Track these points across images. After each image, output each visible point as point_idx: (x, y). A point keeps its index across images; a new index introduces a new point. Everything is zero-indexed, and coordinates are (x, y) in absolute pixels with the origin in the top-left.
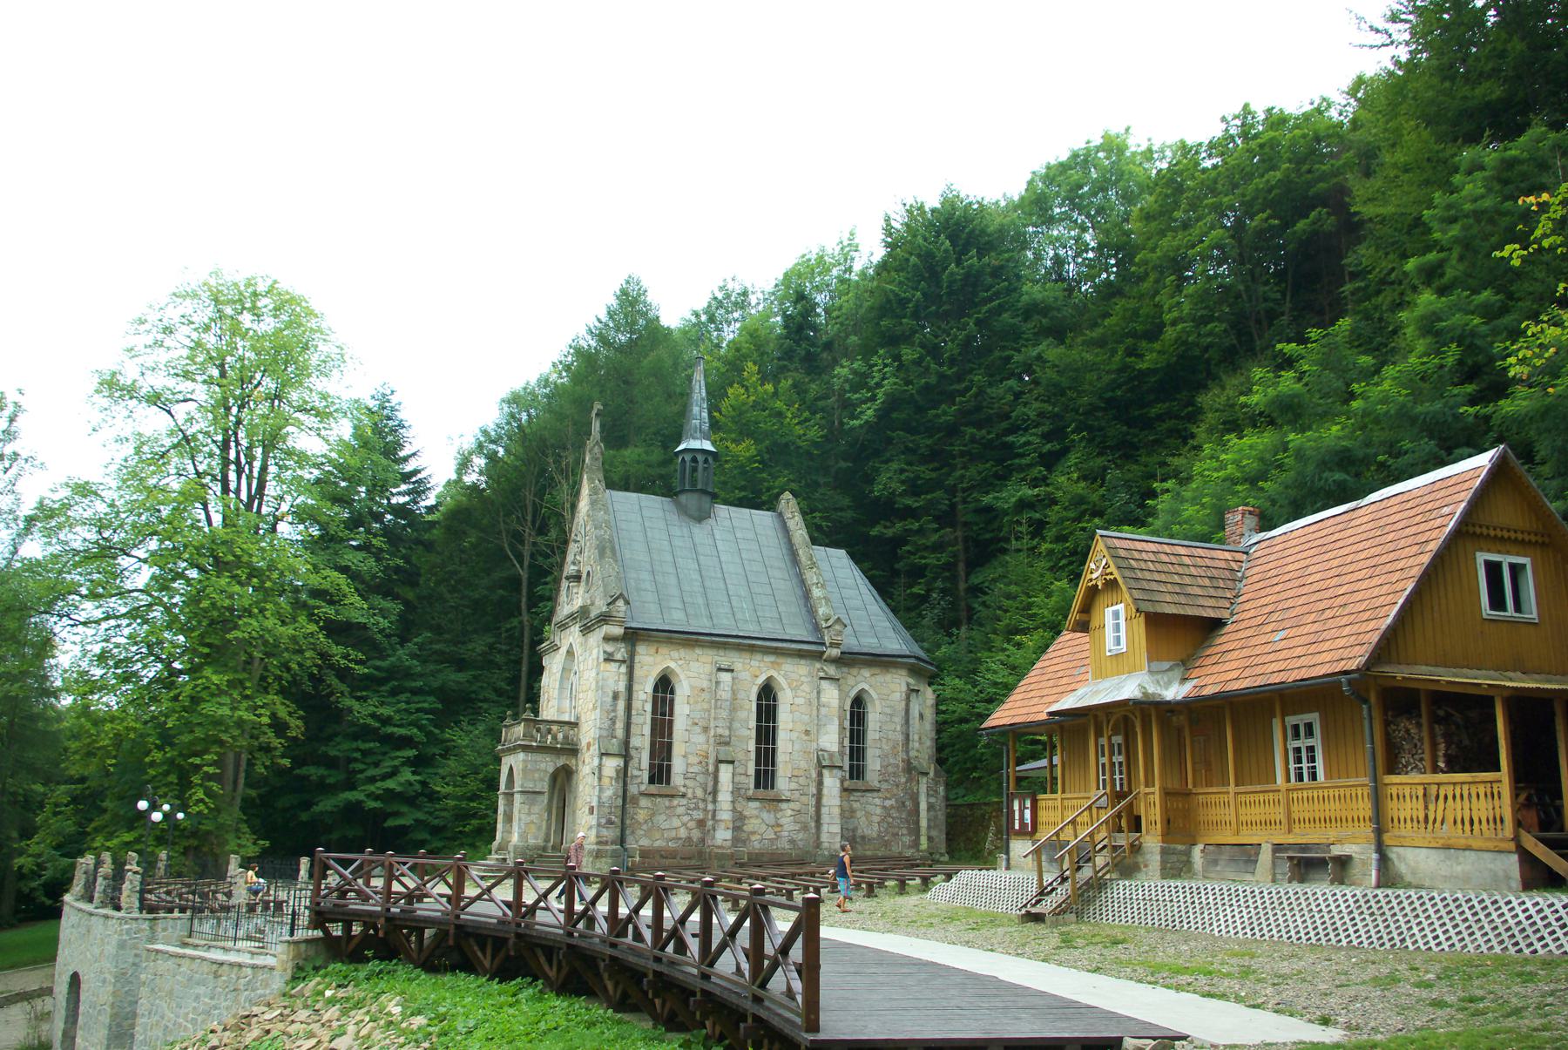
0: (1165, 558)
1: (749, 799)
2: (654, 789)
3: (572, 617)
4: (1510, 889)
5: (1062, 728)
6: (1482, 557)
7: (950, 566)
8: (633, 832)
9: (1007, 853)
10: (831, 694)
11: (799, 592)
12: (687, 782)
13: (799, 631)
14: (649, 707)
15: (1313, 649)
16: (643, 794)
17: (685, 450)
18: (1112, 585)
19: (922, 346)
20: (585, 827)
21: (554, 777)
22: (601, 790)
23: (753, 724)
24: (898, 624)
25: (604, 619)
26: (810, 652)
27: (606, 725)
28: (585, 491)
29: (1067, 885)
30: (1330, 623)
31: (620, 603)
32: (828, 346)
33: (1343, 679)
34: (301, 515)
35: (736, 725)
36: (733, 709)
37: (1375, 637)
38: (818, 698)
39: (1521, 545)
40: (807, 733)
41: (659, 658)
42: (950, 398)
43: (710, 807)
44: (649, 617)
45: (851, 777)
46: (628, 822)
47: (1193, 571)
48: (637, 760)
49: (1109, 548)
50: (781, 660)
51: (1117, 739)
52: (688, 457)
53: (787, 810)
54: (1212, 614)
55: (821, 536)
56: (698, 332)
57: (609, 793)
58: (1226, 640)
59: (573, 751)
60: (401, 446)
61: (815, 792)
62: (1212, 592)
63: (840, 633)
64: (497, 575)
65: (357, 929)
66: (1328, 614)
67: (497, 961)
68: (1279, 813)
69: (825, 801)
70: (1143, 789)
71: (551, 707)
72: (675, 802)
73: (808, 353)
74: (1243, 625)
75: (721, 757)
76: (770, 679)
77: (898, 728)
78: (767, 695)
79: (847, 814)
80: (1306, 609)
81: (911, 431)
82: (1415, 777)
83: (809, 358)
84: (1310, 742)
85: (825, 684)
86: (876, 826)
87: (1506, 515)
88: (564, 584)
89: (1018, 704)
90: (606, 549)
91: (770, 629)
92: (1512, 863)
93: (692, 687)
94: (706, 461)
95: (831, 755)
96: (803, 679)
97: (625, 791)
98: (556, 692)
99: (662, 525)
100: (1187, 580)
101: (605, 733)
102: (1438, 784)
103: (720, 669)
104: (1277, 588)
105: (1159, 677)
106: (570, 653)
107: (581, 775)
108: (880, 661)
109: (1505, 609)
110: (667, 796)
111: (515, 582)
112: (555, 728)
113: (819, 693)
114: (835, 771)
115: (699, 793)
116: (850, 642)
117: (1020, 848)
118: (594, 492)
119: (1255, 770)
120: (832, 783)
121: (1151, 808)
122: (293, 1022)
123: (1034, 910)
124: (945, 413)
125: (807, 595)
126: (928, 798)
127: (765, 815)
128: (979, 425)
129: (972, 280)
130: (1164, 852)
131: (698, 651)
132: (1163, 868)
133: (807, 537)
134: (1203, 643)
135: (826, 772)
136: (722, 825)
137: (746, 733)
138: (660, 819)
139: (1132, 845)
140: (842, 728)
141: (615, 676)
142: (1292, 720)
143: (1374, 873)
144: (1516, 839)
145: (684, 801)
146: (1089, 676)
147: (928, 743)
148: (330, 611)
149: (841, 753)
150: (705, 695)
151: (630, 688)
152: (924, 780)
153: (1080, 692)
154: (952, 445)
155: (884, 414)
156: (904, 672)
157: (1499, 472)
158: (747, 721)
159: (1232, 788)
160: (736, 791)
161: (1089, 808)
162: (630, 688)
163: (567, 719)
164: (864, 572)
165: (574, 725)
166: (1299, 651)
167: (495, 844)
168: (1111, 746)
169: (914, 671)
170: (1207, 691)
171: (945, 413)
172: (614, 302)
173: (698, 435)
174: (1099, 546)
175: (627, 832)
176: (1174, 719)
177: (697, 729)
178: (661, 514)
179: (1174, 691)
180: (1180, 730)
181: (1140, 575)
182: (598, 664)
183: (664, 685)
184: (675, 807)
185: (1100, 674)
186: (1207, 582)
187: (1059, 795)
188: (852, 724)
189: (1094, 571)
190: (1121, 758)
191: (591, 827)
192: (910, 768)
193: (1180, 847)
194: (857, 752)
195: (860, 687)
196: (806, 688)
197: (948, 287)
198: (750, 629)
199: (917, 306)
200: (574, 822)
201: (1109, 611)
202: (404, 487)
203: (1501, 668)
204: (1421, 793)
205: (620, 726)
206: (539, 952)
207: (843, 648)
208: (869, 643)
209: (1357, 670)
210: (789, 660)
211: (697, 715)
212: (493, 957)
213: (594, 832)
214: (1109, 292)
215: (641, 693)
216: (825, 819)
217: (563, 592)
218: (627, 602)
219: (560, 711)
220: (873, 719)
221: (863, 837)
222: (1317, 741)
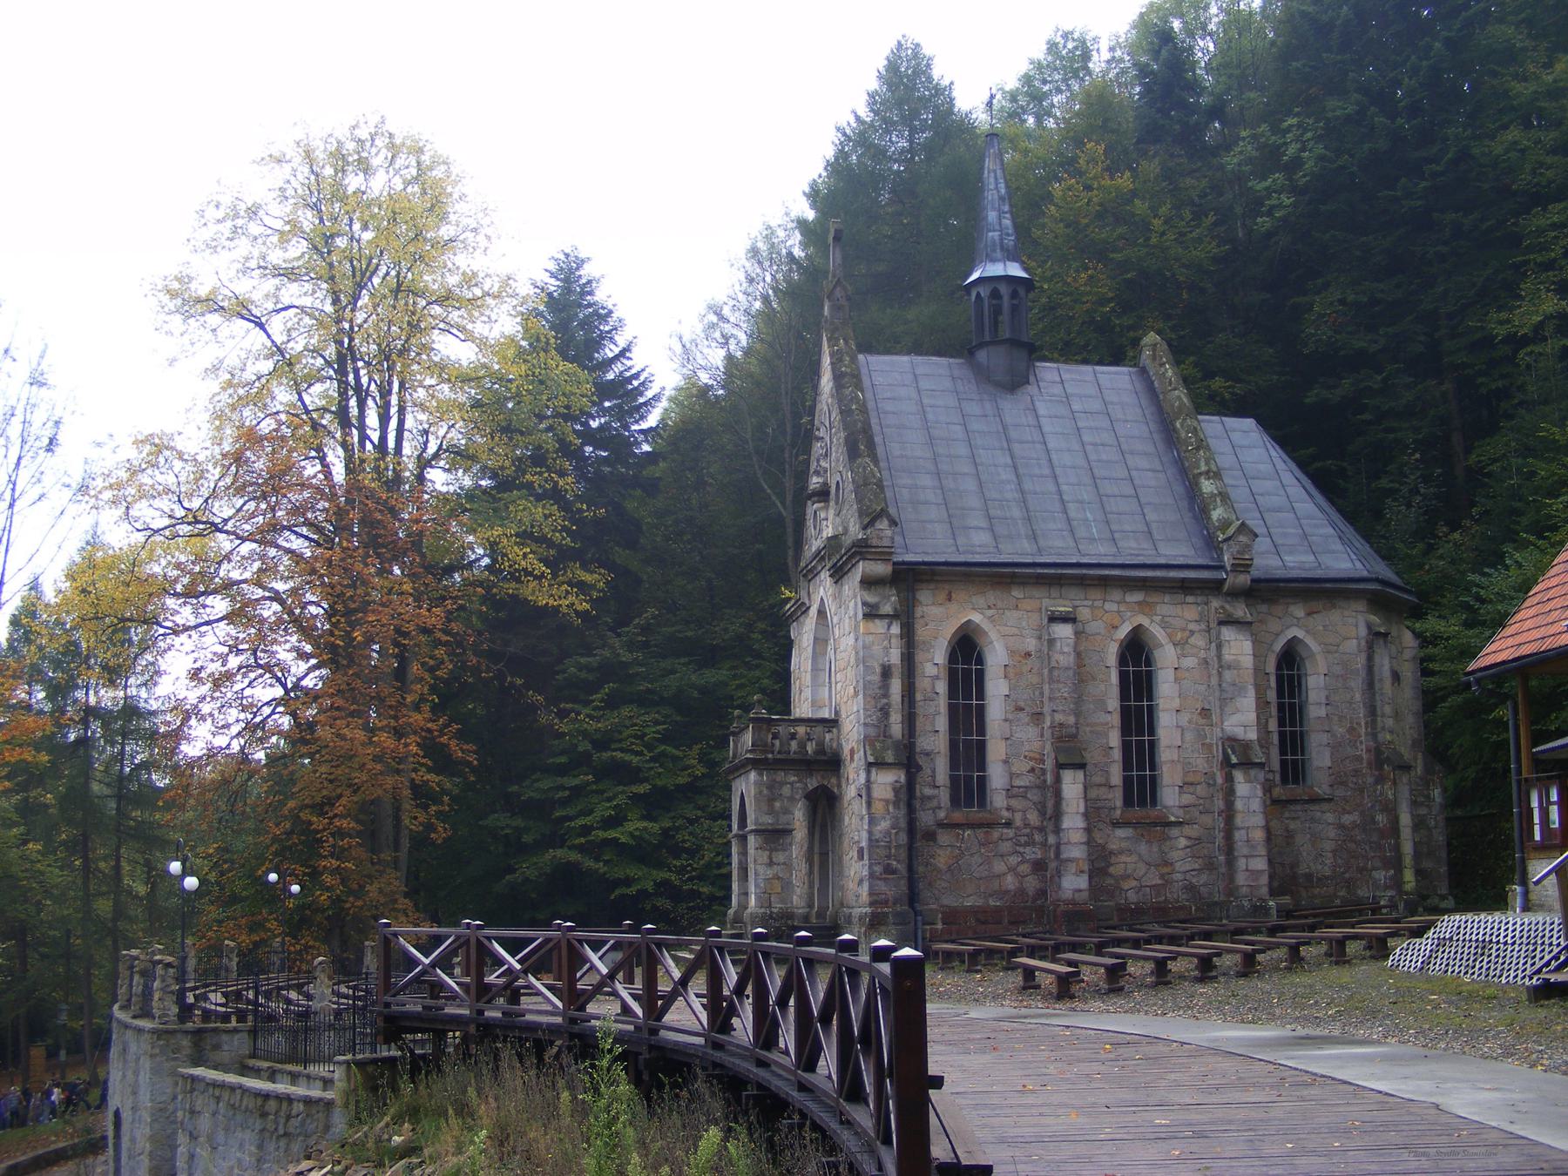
1: (1116, 824)
14: (942, 687)
16: (941, 825)
17: (980, 280)
22: (872, 821)
27: (874, 720)
38: (1219, 656)
41: (953, 607)
45: (1285, 780)
50: (1154, 598)
52: (984, 291)
69: (1239, 820)
76: (1137, 632)
77: (1358, 697)
78: (1136, 652)
79: (1278, 845)
85: (1228, 633)
89: (1528, 624)
93: (1012, 653)
94: (1014, 295)
96: (1192, 626)
101: (872, 732)
106: (822, 613)
113: (1219, 647)
115: (1033, 818)
120: (1248, 792)
127: (1143, 848)
131: (1017, 593)
135: (1239, 776)
136: (1072, 868)
140: (1262, 704)
141: (886, 642)
145: (1010, 833)
149: (1264, 742)
151: (909, 659)
156: (1361, 606)
160: (1093, 813)
162: (909, 659)
173: (999, 254)
183: (966, 649)
195: (1290, 634)
196: (1199, 641)
207: (1255, 573)
208: (1297, 562)
210: (1167, 598)
213: (866, 886)
216: (1241, 849)
218: (893, 523)
220: (1315, 684)
221: (1309, 876)
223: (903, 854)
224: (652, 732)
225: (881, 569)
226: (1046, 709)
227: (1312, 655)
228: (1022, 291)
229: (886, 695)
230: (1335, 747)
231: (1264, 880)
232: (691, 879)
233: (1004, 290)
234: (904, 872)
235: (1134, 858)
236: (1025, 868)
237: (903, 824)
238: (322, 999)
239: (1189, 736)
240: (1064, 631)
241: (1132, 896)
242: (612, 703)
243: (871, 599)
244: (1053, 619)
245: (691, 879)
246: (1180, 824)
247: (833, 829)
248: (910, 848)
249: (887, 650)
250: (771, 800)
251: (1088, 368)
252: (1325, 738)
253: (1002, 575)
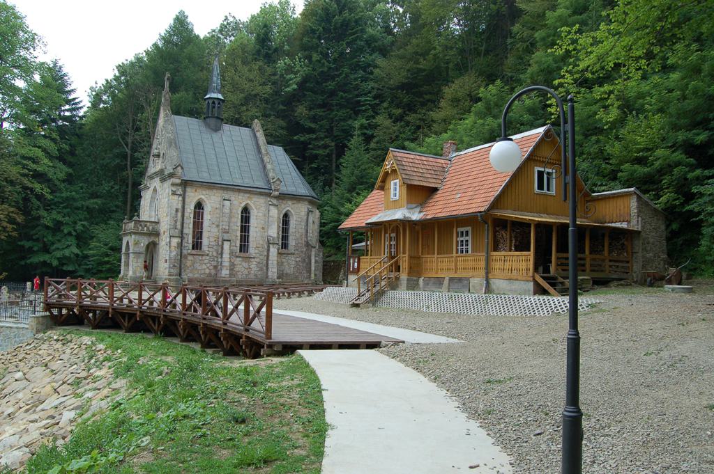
0: (416, 161)
1: (237, 257)
2: (194, 252)
3: (156, 174)
4: (529, 294)
5: (372, 230)
6: (537, 169)
7: (329, 155)
8: (185, 271)
9: (347, 280)
10: (274, 212)
11: (261, 166)
12: (210, 249)
14: (192, 216)
15: (470, 202)
16: (189, 254)
17: (210, 98)
18: (394, 171)
19: (321, 53)
20: (163, 269)
21: (148, 247)
23: (239, 224)
24: (305, 182)
25: (171, 175)
27: (173, 224)
28: (162, 114)
29: (370, 292)
30: (477, 192)
31: (179, 168)
32: (276, 50)
33: (479, 214)
34: (15, 118)
35: (231, 224)
36: (230, 217)
37: (492, 199)
39: (551, 164)
40: (263, 228)
42: (333, 78)
43: (220, 260)
44: (192, 175)
45: (282, 248)
46: (183, 266)
47: (428, 167)
48: (186, 239)
49: (394, 156)
50: (252, 196)
51: (393, 235)
52: (211, 101)
53: (254, 262)
54: (433, 186)
55: (272, 140)
56: (214, 40)
57: (174, 254)
58: (438, 196)
59: (157, 234)
60: (66, 86)
61: (266, 254)
62: (435, 176)
63: (279, 185)
64: (116, 151)
65: (64, 311)
66: (477, 188)
67: (130, 324)
68: (452, 265)
69: (270, 258)
70: (401, 255)
71: (146, 213)
72: (204, 258)
73: (267, 54)
74: (445, 190)
75: (225, 238)
79: (280, 264)
80: (469, 186)
81: (314, 92)
82: (503, 253)
83: (267, 56)
84: (467, 238)
85: (271, 207)
86: (292, 270)
87: (547, 153)
88: (152, 158)
89: (354, 219)
90: (173, 143)
91: (247, 182)
92: (531, 286)
94: (219, 104)
95: (274, 238)
97: (181, 253)
98: (148, 208)
100: (425, 171)
102: (505, 256)
103: (224, 200)
104: (460, 176)
105: (410, 210)
106: (155, 190)
107: (160, 246)
108: (296, 198)
109: (543, 189)
110: (200, 255)
111: (125, 156)
112: (148, 224)
113: (269, 211)
114: (275, 245)
115: (215, 254)
116: (283, 189)
117: (352, 278)
118: (166, 115)
119: (445, 249)
120: (274, 251)
121: (405, 265)
122: (40, 349)
123: (356, 302)
124: (330, 85)
125: (265, 167)
126: (316, 258)
127: (244, 264)
128: (344, 92)
129: (346, 25)
130: (408, 280)
131: (215, 191)
132: (407, 286)
133: (265, 141)
134: (427, 199)
135: (271, 246)
136: (225, 268)
137: (236, 228)
138: (197, 265)
139: (396, 277)
140: (279, 227)
141: (176, 202)
142: (460, 230)
143: (484, 289)
144: (533, 276)
145: (208, 258)
146: (383, 208)
147: (316, 234)
148: (34, 166)
149: (278, 238)
150: (218, 211)
151: (183, 207)
152: (313, 250)
153: (379, 215)
154: (332, 100)
155: (302, 85)
156: (307, 203)
157: (547, 133)
158: (237, 222)
159: (436, 255)
160: (231, 253)
161: (380, 262)
162: (183, 207)
163: (153, 220)
164: (290, 158)
165: (157, 223)
166: (464, 203)
167: (120, 276)
168: (391, 238)
169: (311, 202)
170: (429, 217)
171: (330, 85)
173: (216, 91)
174: (390, 155)
175: (183, 270)
176: (417, 227)
177: (214, 226)
179: (416, 216)
180: (418, 233)
181: (406, 168)
182: (169, 196)
183: (199, 206)
184: (203, 260)
185: (387, 208)
186: (433, 172)
187: (369, 257)
188: (283, 225)
189: (388, 165)
190: (394, 243)
191: (166, 269)
192: (308, 245)
193: (415, 278)
194: (285, 238)
195: (288, 208)
196: (263, 209)
197: (335, 25)
198: (239, 182)
199: (320, 33)
200: (157, 267)
201: (393, 182)
202: (67, 107)
203: (539, 212)
204: (503, 259)
205: (179, 224)
206: (150, 319)
207: (280, 192)
208: (291, 190)
209: (485, 211)
210: (256, 196)
211: (215, 220)
212: (128, 322)
213: (167, 270)
214: (409, 34)
215: (189, 209)
216: (270, 266)
217: (151, 162)
218: (182, 168)
219: (150, 217)
220: (293, 223)
221: (287, 274)
222: (469, 238)
223: (179, 262)
225: (178, 181)
226: (221, 224)
228: (221, 103)
231: (276, 274)
234: (178, 266)
235: (241, 266)
236: (212, 267)
237: (179, 253)
238: (4, 299)
240: (227, 203)
241: (240, 276)
243: (174, 189)
246: (254, 258)
247: (155, 253)
248: (180, 260)
251: (237, 127)
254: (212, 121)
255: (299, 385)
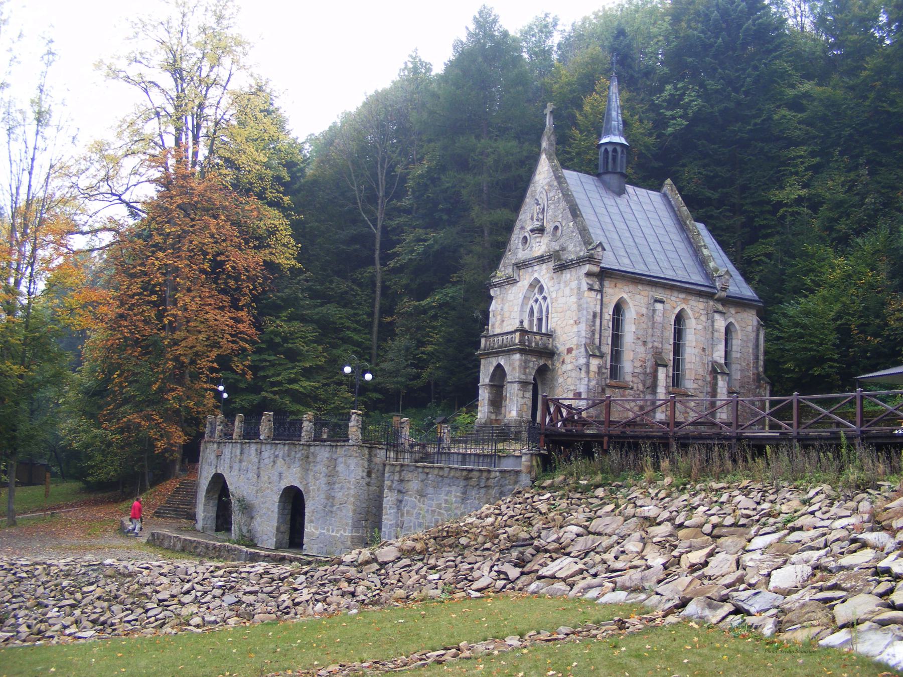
13: (697, 277)
22: (589, 381)
26: (706, 295)
27: (589, 336)
38: (713, 326)
41: (617, 290)
44: (609, 261)
50: (689, 297)
52: (610, 148)
72: (628, 392)
76: (682, 310)
77: (751, 351)
78: (680, 319)
85: (717, 316)
93: (637, 313)
96: (702, 312)
99: (597, 196)
101: (588, 341)
113: (713, 322)
131: (640, 287)
135: (719, 377)
145: (632, 392)
172: (472, 27)
173: (617, 132)
178: (595, 188)
183: (618, 309)
196: (703, 318)
210: (693, 298)
224: (310, 336)
225: (596, 269)
227: (736, 331)
229: (594, 325)
230: (742, 371)
232: (325, 414)
233: (619, 149)
239: (698, 359)
240: (659, 306)
242: (290, 319)
244: (657, 301)
245: (325, 414)
246: (692, 396)
249: (596, 305)
250: (525, 368)
252: (739, 367)
253: (636, 278)
254: (613, 179)
255: (254, 558)
